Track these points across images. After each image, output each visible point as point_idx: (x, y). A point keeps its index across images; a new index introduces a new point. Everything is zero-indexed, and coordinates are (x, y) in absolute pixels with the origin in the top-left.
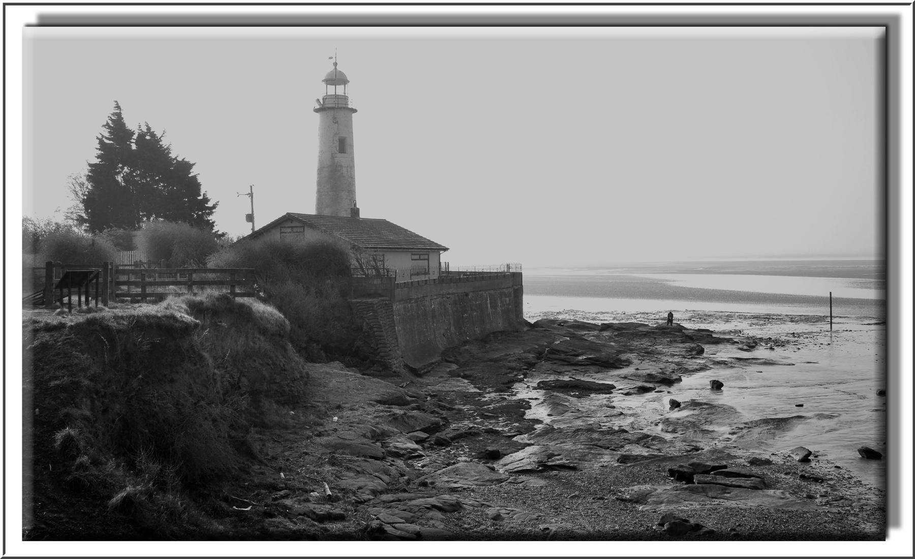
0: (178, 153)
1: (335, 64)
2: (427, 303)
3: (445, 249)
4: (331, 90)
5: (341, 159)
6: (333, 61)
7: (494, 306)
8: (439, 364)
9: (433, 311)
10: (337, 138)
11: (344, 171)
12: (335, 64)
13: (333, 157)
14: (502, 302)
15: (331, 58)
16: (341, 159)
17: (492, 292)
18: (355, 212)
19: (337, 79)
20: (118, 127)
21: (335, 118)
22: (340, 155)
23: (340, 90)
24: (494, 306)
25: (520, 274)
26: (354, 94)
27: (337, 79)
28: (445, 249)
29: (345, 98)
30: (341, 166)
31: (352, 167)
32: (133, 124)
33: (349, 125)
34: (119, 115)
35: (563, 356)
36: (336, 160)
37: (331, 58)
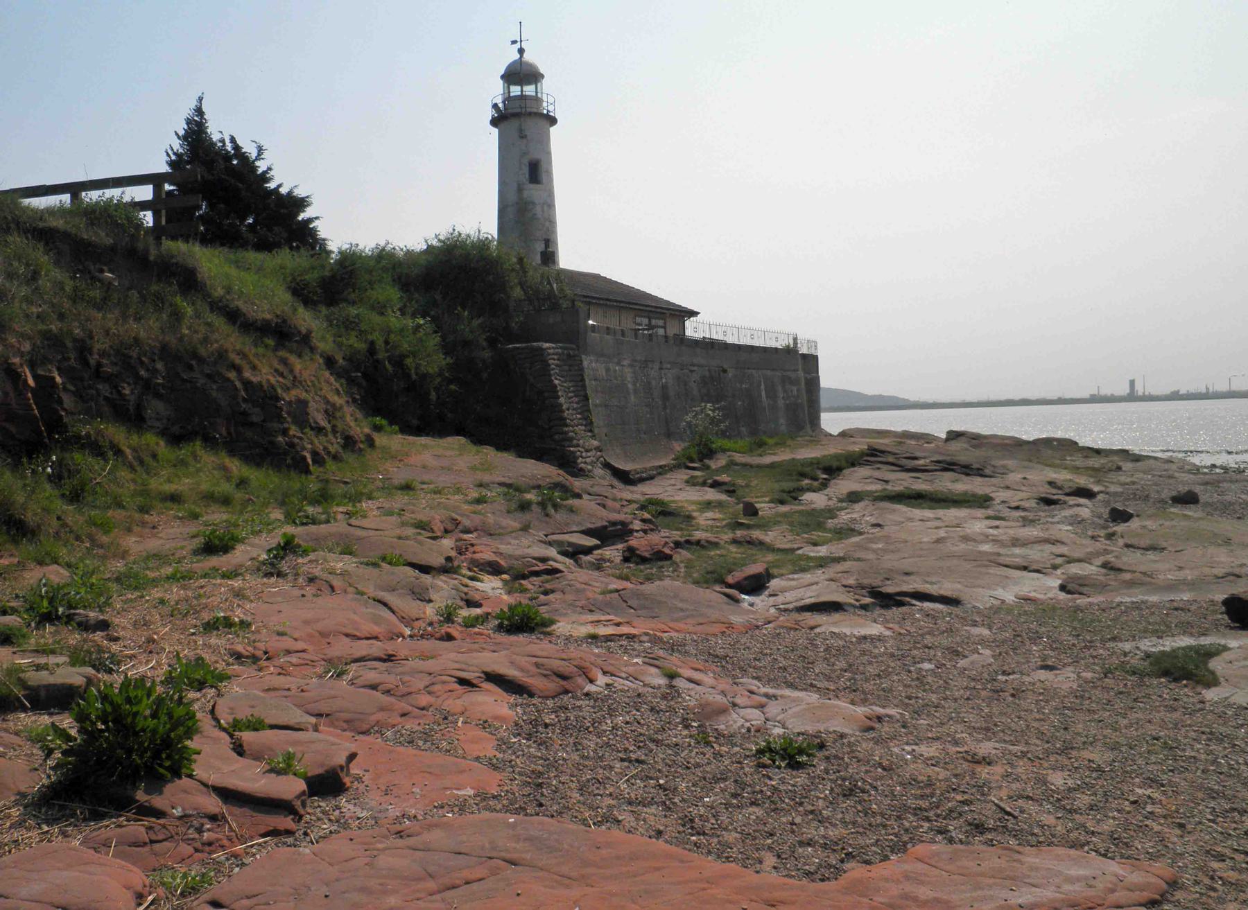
0: (284, 179)
1: (521, 51)
2: (653, 373)
3: (693, 314)
4: (515, 90)
5: (532, 192)
6: (518, 45)
7: (772, 394)
8: (672, 468)
9: (664, 387)
10: (526, 161)
11: (538, 209)
12: (521, 51)
13: (520, 190)
14: (785, 391)
15: (514, 42)
16: (532, 192)
17: (769, 373)
18: (549, 257)
19: (520, 73)
20: (196, 133)
21: (521, 131)
22: (532, 186)
23: (529, 90)
24: (772, 394)
25: (815, 358)
26: (553, 92)
27: (520, 73)
28: (693, 314)
29: (537, 100)
30: (533, 203)
31: (550, 205)
32: (217, 130)
33: (545, 141)
34: (199, 111)
35: (891, 459)
36: (526, 194)
37: (514, 42)
